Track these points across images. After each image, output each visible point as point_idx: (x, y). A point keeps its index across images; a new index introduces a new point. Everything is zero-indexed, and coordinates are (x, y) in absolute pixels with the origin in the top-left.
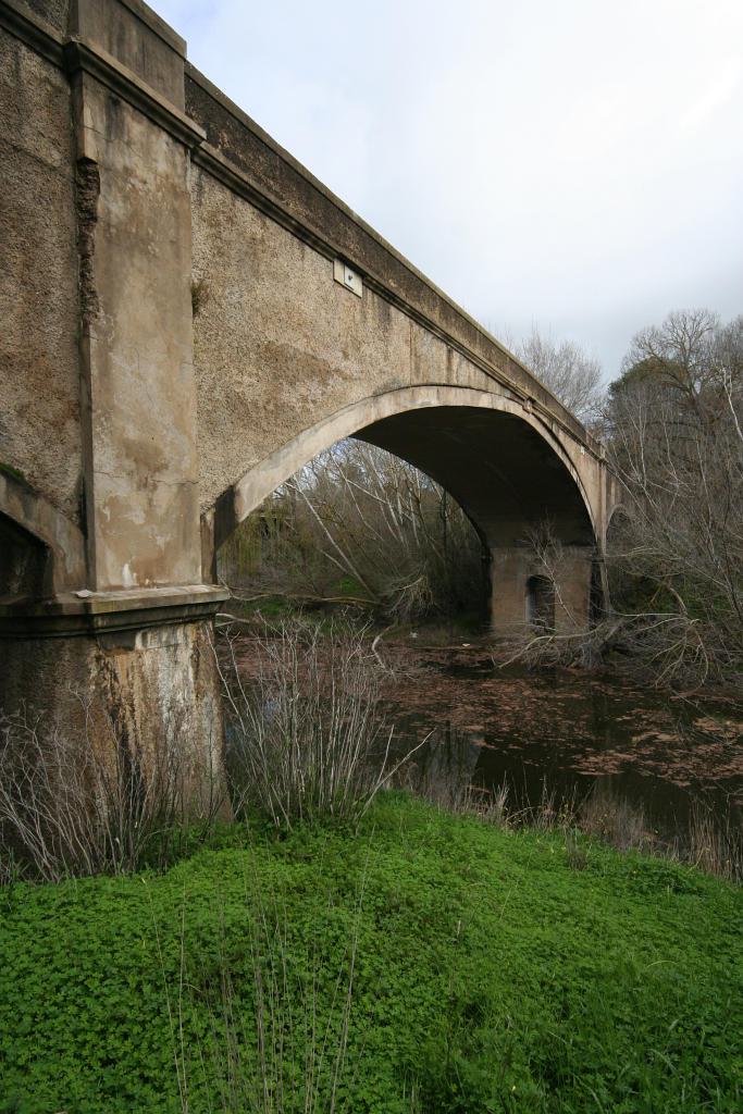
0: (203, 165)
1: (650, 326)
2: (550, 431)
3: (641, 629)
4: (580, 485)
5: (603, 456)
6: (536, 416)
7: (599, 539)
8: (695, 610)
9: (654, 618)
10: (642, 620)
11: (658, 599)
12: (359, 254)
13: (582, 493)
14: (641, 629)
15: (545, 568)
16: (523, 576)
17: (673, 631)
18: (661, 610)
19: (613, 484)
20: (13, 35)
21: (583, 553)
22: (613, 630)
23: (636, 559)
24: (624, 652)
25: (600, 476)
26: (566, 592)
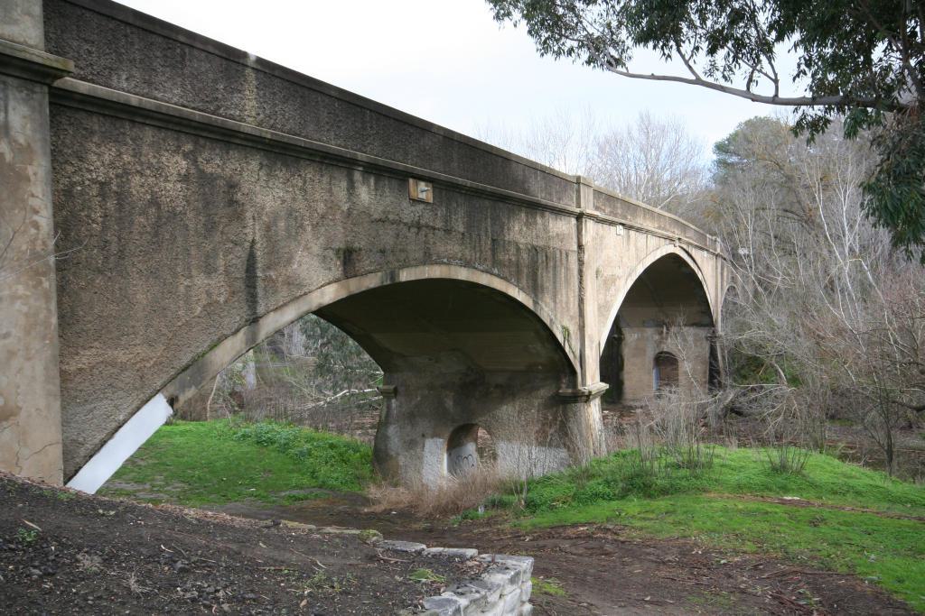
0: (226, 139)
1: (550, 57)
2: (687, 252)
3: (753, 396)
4: (703, 283)
5: (719, 251)
6: (682, 248)
7: (716, 321)
8: (794, 380)
9: (762, 388)
10: (753, 390)
11: (765, 372)
12: (442, 170)
13: (705, 287)
14: (753, 396)
15: (672, 344)
16: (651, 354)
17: (775, 397)
18: (767, 381)
19: (725, 269)
20: (86, 111)
21: (703, 333)
22: (731, 396)
23: (749, 341)
24: (739, 413)
25: (716, 268)
26: (690, 367)
